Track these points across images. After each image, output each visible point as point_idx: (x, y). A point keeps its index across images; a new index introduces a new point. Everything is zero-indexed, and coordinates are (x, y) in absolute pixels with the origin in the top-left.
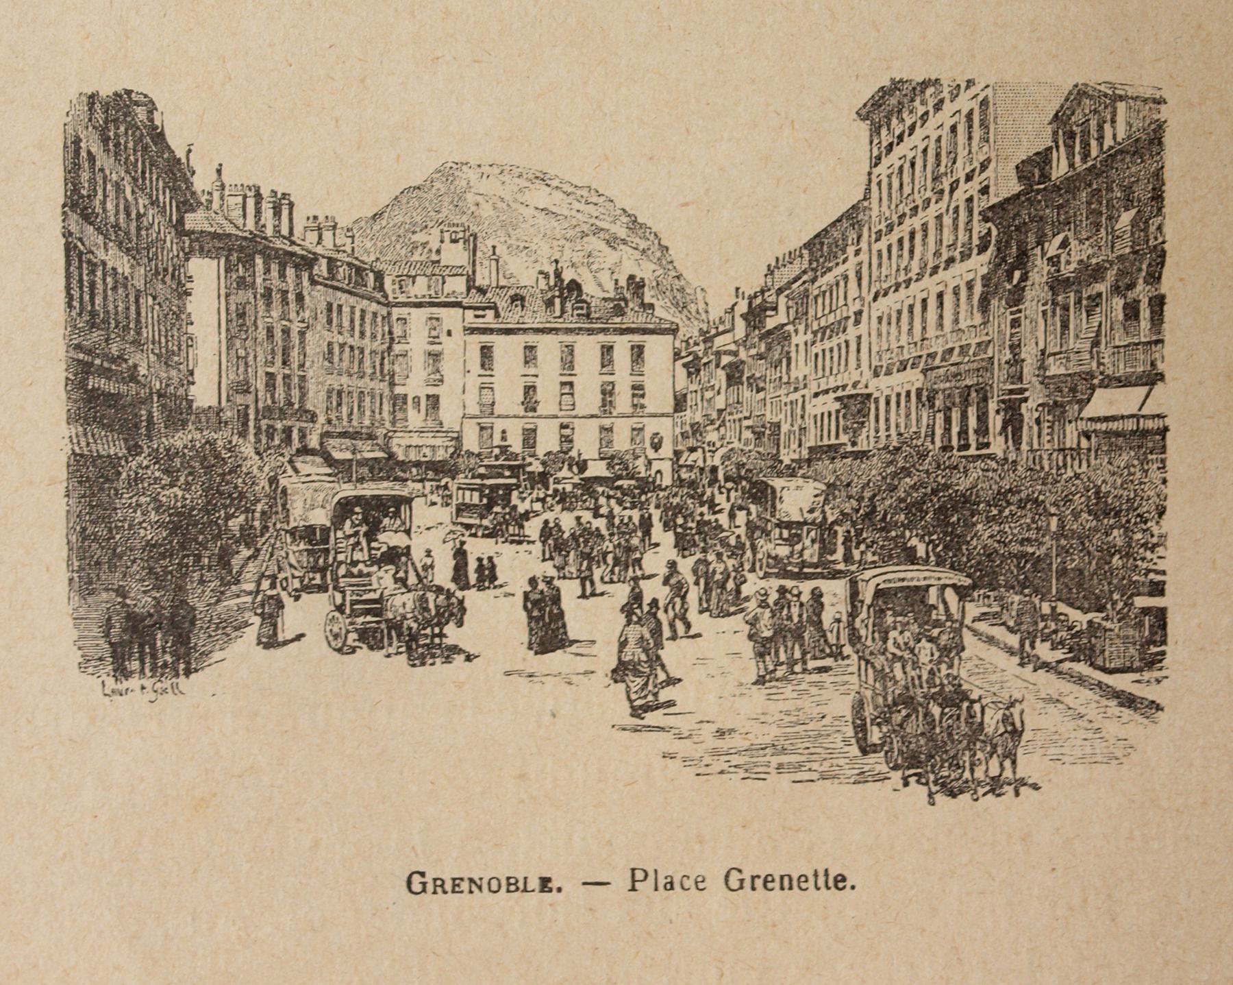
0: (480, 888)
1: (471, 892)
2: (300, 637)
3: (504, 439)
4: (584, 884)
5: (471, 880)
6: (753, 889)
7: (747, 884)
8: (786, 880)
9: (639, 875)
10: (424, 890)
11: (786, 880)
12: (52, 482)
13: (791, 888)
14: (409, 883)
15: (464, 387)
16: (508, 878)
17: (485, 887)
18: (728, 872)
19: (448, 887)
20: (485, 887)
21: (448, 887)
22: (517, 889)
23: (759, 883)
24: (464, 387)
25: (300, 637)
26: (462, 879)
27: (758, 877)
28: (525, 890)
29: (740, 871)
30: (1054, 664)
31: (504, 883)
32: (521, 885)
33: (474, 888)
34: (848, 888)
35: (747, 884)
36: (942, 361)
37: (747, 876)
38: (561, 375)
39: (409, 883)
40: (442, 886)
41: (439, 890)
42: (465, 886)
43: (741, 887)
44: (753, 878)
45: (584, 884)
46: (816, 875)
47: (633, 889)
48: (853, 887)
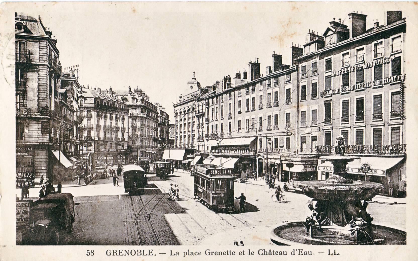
0: (128, 254)
6: (230, 255)
7: (211, 254)
8: (220, 253)
9: (185, 254)
10: (209, 254)
11: (220, 253)
12: (382, 89)
13: (221, 255)
14: (291, 253)
15: (288, 245)
17: (130, 254)
18: (259, 251)
19: (118, 253)
20: (130, 254)
22: (141, 254)
23: (213, 254)
24: (288, 245)
29: (209, 250)
33: (126, 254)
35: (211, 254)
36: (353, 37)
38: (284, 252)
39: (291, 253)
41: (115, 254)
44: (212, 252)
46: (227, 252)
47: (184, 257)
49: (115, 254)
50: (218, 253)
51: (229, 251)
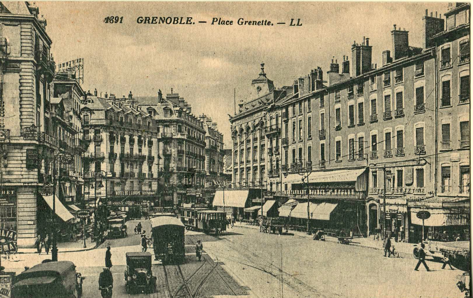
1: (159, 23)
2: (416, 269)
3: (347, 59)
4: (200, 22)
5: (161, 18)
7: (244, 23)
9: (215, 20)
16: (175, 18)
19: (151, 21)
21: (151, 21)
23: (247, 23)
25: (416, 269)
26: (157, 18)
27: (247, 22)
28: (181, 23)
29: (243, 19)
30: (199, 119)
31: (225, 23)
32: (179, 21)
34: (192, 23)
35: (244, 23)
37: (244, 21)
40: (148, 20)
41: (147, 21)
42: (158, 20)
43: (242, 24)
45: (200, 22)
47: (213, 24)
48: (194, 23)
49: (147, 21)
50: (252, 23)
51: (264, 21)
